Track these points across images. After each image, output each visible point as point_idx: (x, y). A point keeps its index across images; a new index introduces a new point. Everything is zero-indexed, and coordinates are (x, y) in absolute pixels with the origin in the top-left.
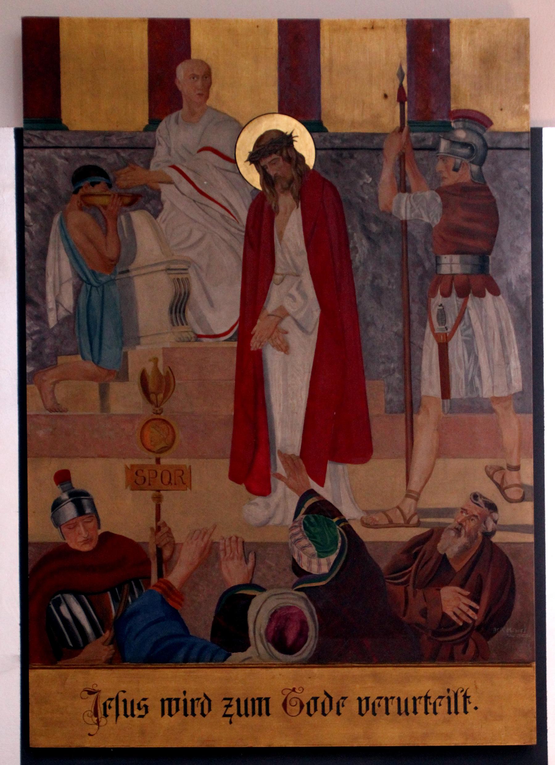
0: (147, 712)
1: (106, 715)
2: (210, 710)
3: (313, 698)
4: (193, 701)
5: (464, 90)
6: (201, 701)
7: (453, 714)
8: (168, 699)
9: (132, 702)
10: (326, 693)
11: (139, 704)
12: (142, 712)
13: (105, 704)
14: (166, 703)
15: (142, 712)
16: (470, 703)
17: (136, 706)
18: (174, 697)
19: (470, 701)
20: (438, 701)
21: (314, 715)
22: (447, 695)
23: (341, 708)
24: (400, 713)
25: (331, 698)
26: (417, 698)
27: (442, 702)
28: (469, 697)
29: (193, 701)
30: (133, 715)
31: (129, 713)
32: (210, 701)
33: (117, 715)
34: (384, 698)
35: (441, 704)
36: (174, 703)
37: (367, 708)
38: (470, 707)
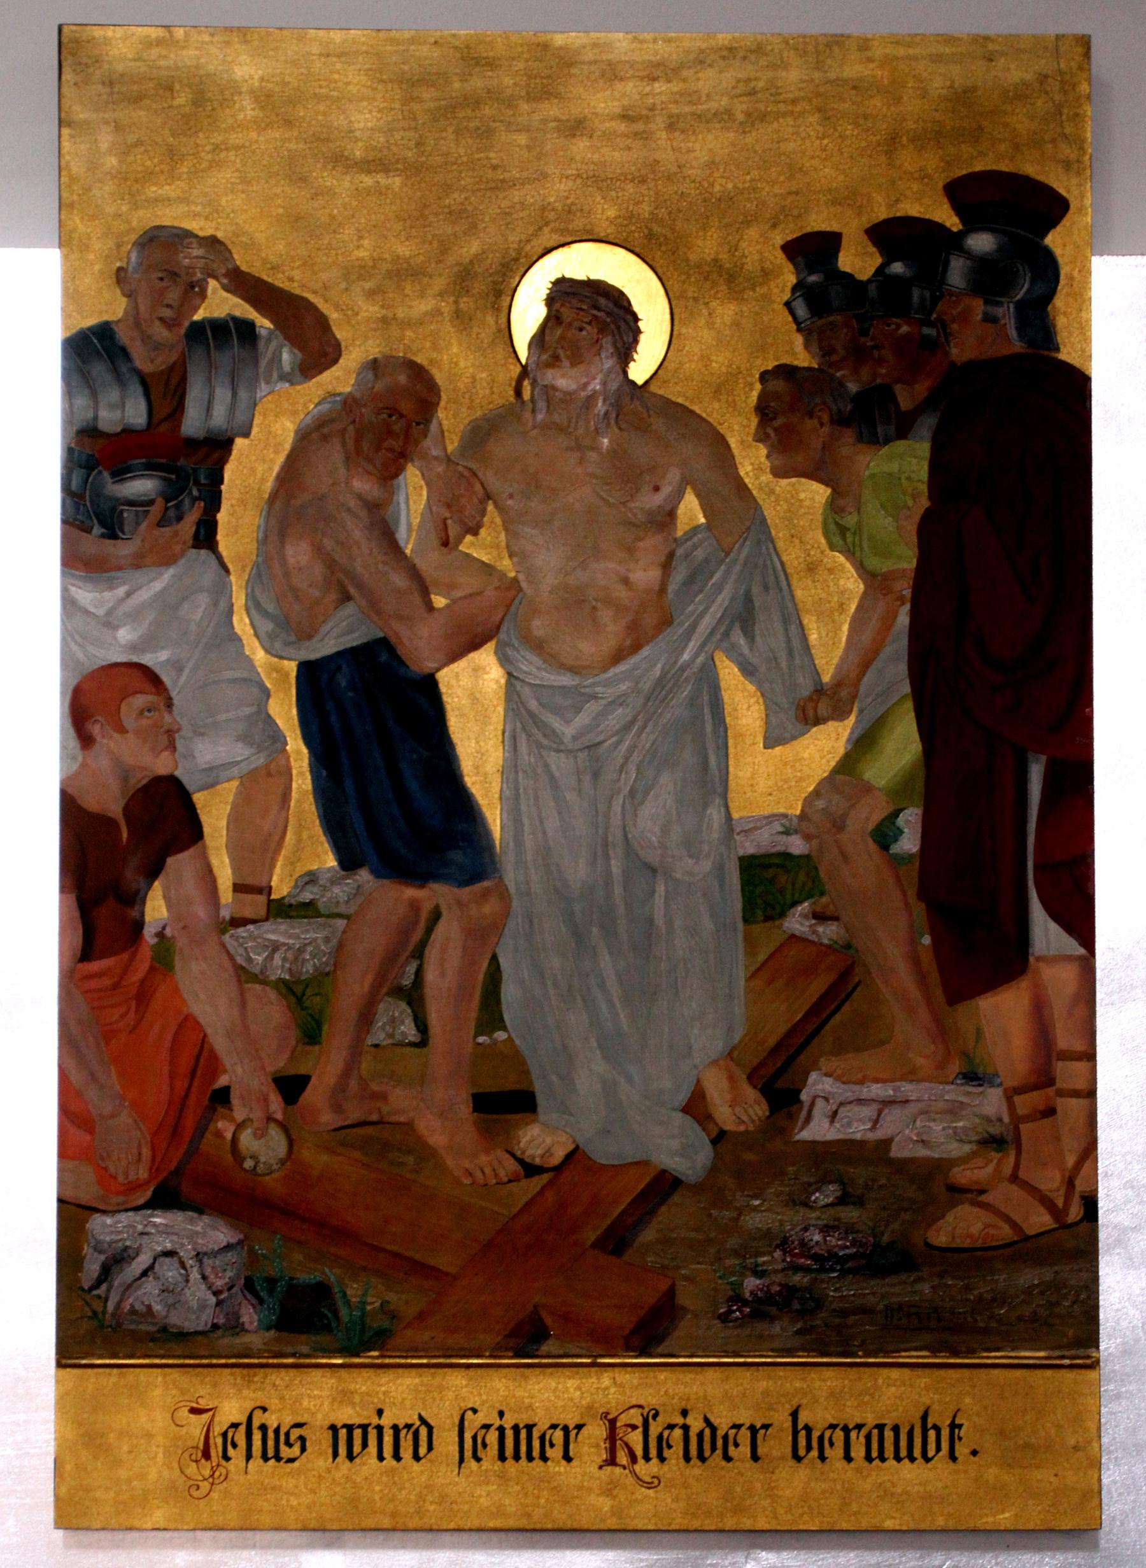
0: (303, 1449)
1: (227, 1458)
2: (430, 1448)
3: (877, 1426)
4: (516, 1429)
5: (841, 178)
6: (864, 1432)
7: (695, 1461)
8: (344, 1426)
9: (277, 1431)
10: (707, 1420)
11: (287, 1434)
12: (296, 1450)
13: (224, 1435)
14: (343, 1433)
15: (296, 1450)
16: (960, 1439)
17: (282, 1438)
18: (357, 1421)
19: (962, 1434)
20: (827, 1434)
21: (711, 1459)
22: (497, 1423)
23: (731, 1448)
24: (869, 1458)
25: (714, 1430)
26: (401, 1427)
27: (488, 1441)
28: (960, 1426)
29: (516, 1429)
30: (278, 1458)
31: (903, 1453)
32: (430, 1429)
33: (249, 1456)
34: (492, 1428)
35: (739, 1441)
36: (357, 1433)
37: (809, 1448)
38: (961, 1450)
